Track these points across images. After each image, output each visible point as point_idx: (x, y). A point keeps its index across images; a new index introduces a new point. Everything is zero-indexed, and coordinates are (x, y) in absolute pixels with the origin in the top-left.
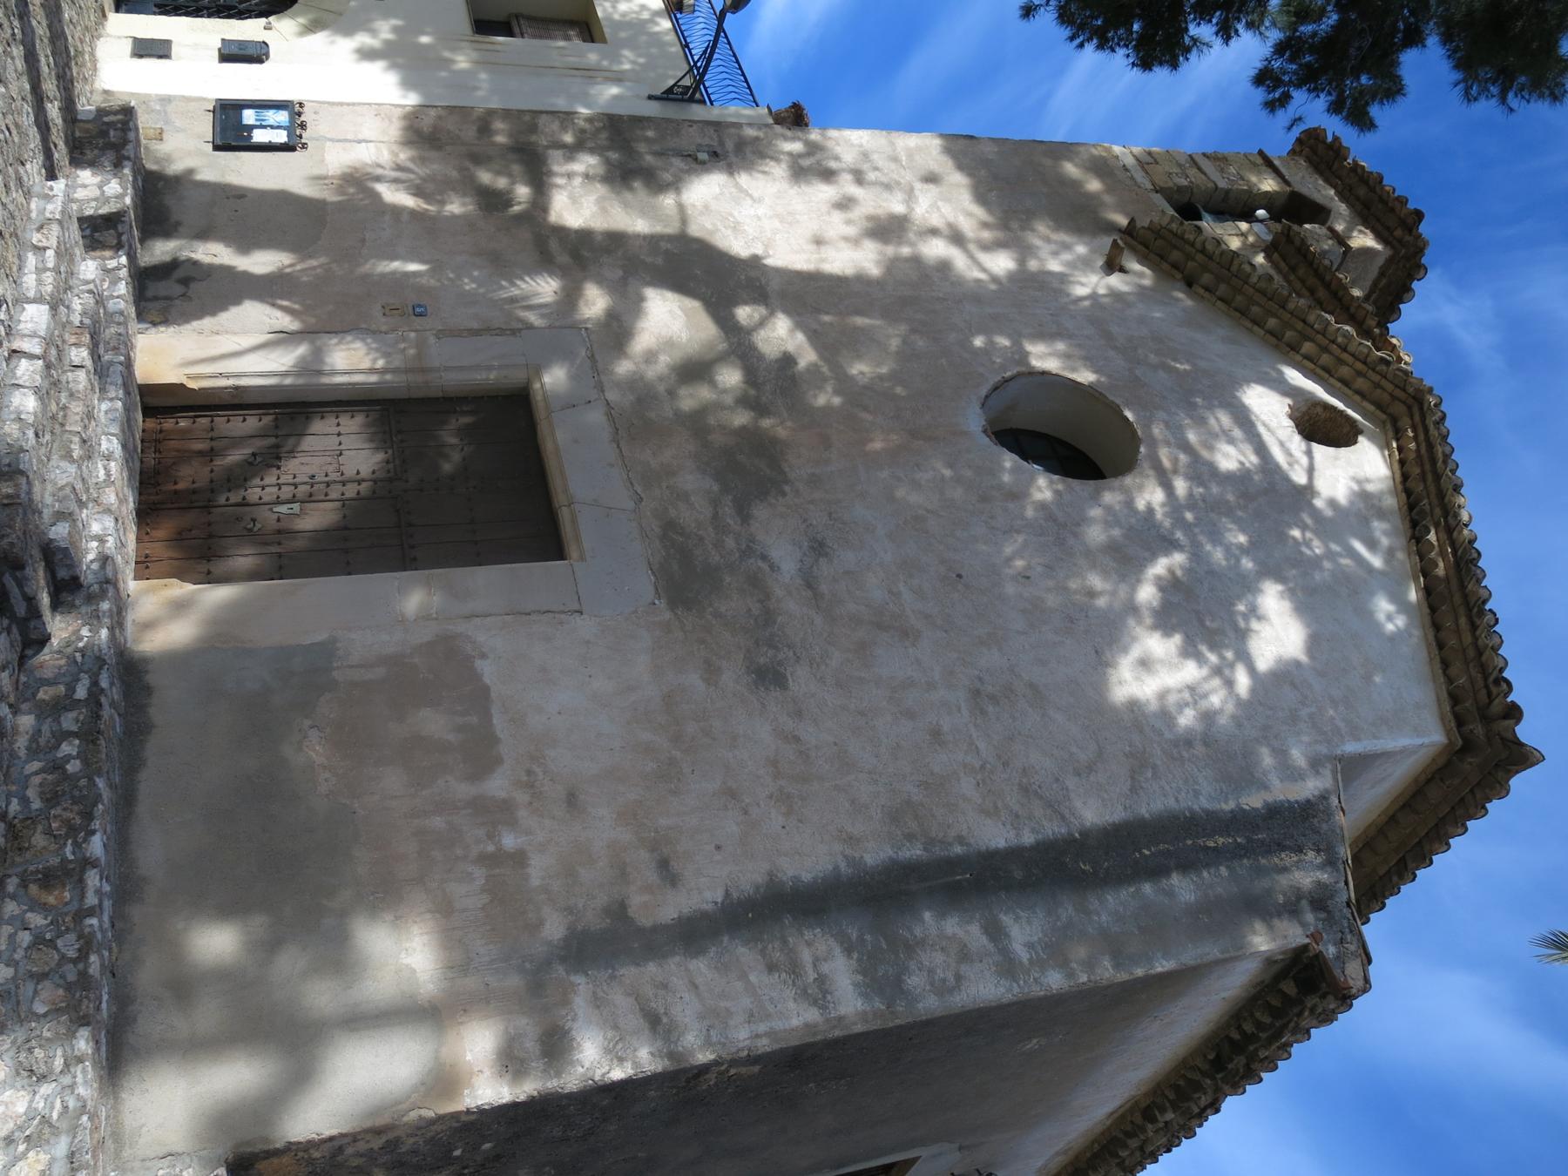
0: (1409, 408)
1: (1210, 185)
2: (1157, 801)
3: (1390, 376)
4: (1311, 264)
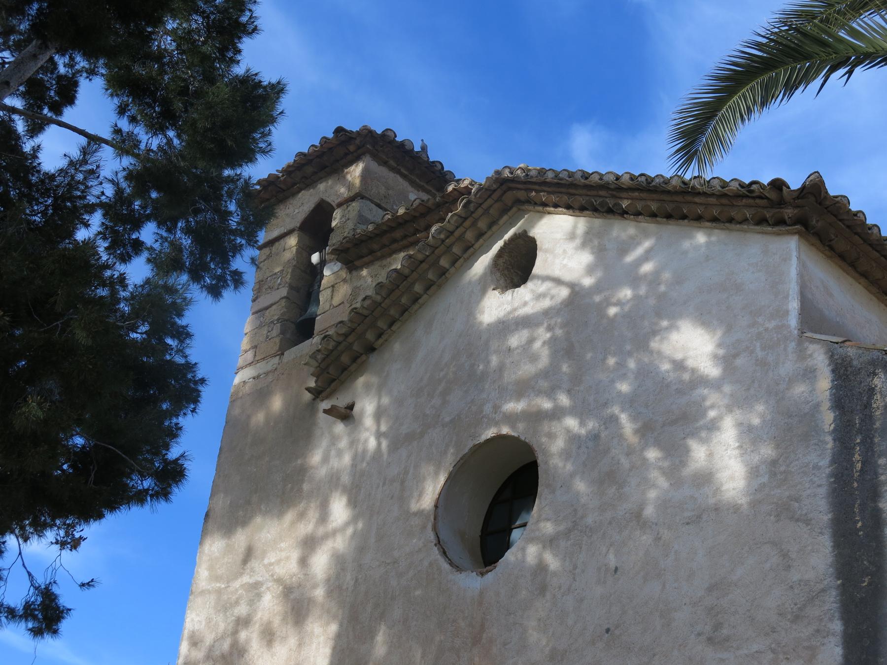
0: (510, 189)
1: (283, 303)
2: (818, 504)
3: (480, 201)
4: (370, 238)
